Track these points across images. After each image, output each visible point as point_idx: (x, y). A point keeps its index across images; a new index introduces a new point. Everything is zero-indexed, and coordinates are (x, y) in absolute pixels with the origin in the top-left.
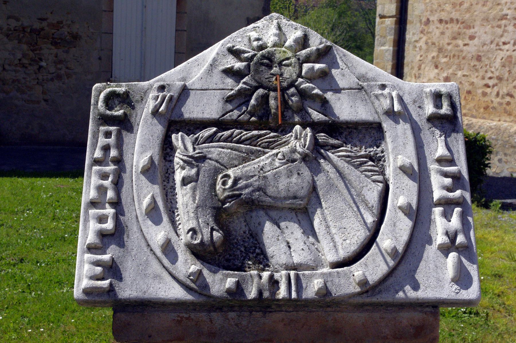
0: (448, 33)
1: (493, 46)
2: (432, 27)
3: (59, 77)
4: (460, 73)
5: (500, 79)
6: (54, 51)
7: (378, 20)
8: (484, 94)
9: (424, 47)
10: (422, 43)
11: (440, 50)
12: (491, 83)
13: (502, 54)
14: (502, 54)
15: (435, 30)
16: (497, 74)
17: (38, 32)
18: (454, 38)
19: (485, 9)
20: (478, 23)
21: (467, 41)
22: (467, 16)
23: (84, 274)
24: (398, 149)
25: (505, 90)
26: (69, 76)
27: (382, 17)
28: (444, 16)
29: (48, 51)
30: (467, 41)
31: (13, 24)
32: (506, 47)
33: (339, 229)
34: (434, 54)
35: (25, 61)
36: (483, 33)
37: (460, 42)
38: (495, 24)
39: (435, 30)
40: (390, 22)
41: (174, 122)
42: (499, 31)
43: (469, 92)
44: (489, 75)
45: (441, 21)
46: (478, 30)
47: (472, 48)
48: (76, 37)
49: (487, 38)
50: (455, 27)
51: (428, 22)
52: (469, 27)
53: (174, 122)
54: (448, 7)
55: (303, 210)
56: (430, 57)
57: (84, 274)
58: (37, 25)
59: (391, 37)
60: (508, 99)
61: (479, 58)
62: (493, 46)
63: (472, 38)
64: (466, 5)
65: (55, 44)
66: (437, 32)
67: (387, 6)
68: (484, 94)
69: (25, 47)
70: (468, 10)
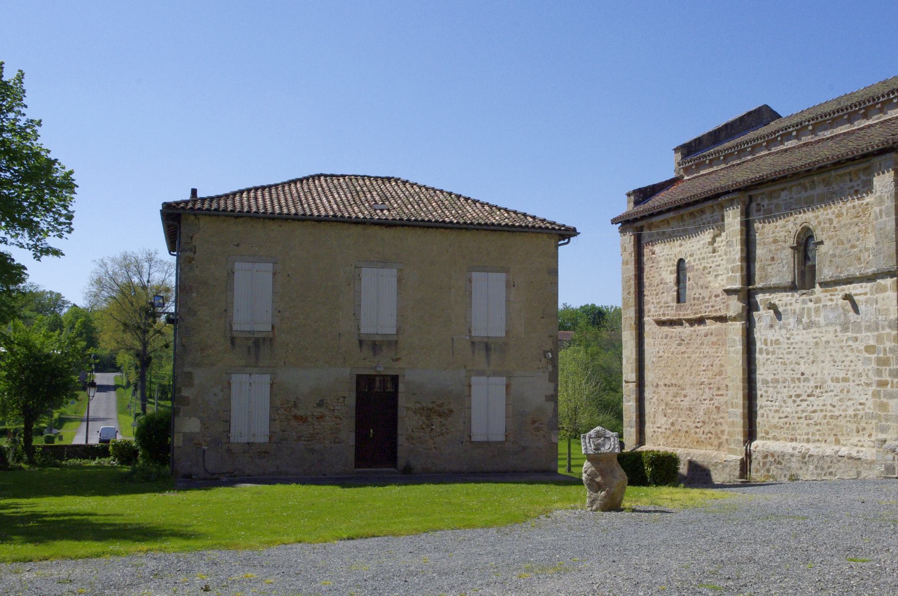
0: (671, 393)
1: (698, 401)
2: (660, 389)
3: (442, 434)
4: (680, 420)
5: (704, 422)
6: (440, 420)
7: (624, 383)
8: (696, 433)
9: (656, 402)
10: (654, 400)
11: (667, 404)
12: (699, 425)
13: (704, 407)
14: (704, 407)
15: (662, 390)
16: (702, 419)
17: (431, 409)
18: (675, 397)
19: (692, 378)
20: (688, 387)
21: (683, 398)
22: (681, 382)
23: (583, 452)
24: (612, 439)
25: (707, 430)
26: (447, 433)
27: (627, 382)
28: (667, 382)
29: (436, 420)
30: (683, 398)
31: (418, 406)
32: (706, 402)
33: (607, 447)
34: (663, 407)
35: (424, 426)
36: (692, 393)
37: (679, 399)
38: (698, 387)
39: (662, 390)
40: (632, 386)
41: (590, 438)
42: (701, 392)
43: (686, 432)
44: (698, 420)
45: (665, 385)
46: (688, 391)
47: (686, 403)
48: (451, 411)
49: (695, 397)
50: (675, 389)
51: (657, 385)
52: (683, 389)
53: (590, 438)
54: (669, 376)
55: (604, 445)
56: (660, 410)
57: (583, 452)
58: (430, 406)
59: (633, 397)
60: (710, 435)
61: (690, 409)
62: (698, 401)
63: (685, 396)
64: (680, 375)
65: (440, 415)
66: (664, 393)
67: (629, 375)
68: (696, 433)
69: (424, 418)
70: (682, 377)
